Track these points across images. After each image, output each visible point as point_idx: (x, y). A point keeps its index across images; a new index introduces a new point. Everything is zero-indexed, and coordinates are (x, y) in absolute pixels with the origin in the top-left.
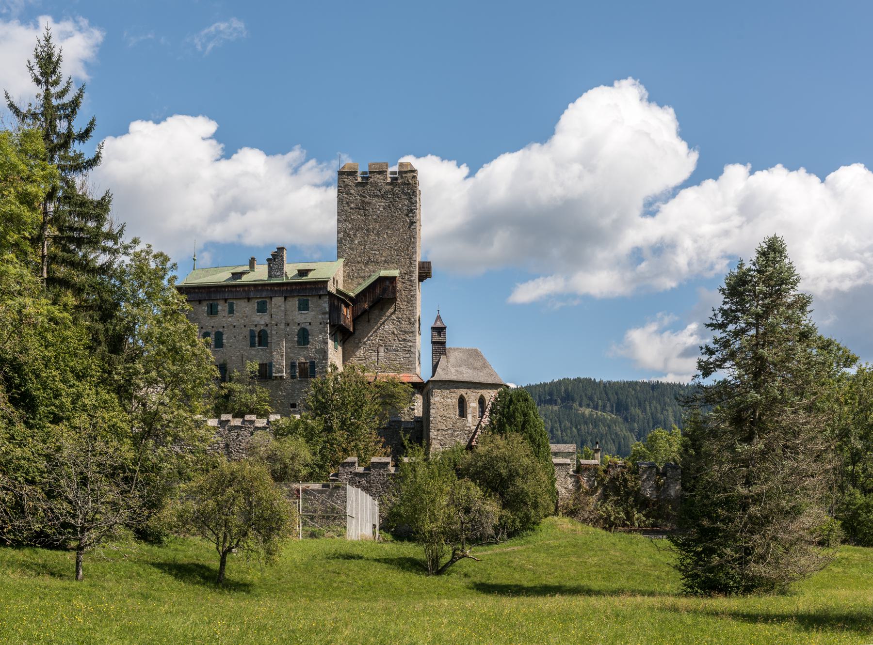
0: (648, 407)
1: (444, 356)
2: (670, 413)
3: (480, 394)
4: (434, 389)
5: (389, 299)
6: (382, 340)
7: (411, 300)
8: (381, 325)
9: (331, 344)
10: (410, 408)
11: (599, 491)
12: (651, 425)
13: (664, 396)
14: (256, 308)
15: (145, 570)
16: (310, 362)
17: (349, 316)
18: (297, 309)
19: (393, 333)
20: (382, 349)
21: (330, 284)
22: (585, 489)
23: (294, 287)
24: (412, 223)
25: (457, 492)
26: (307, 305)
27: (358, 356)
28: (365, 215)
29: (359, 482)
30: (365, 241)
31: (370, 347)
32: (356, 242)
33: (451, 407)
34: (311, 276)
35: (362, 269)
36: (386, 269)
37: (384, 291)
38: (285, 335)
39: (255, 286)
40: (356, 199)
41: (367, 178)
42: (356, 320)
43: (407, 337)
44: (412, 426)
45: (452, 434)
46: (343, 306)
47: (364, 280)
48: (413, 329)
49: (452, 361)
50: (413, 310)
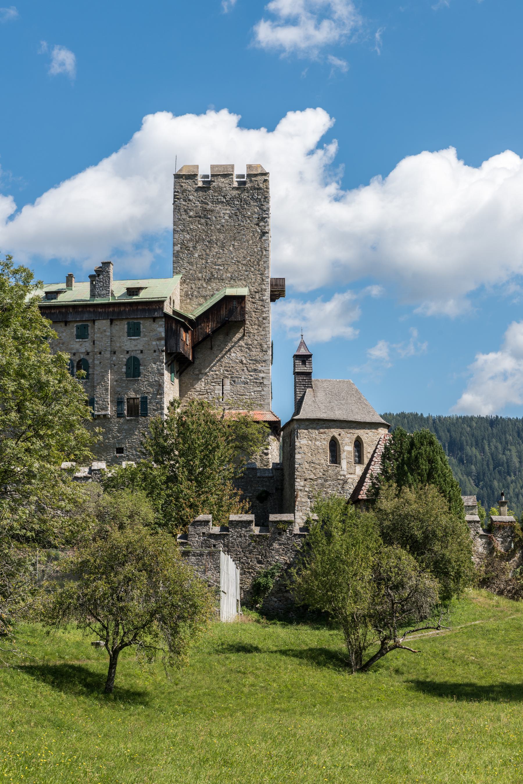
0: (487, 448)
1: (310, 389)
2: (514, 454)
3: (356, 436)
4: (300, 429)
5: (236, 322)
6: (227, 371)
7: (263, 322)
8: (227, 352)
9: (167, 375)
10: (263, 453)
11: (518, 555)
12: (491, 467)
13: (505, 433)
14: (75, 333)
15: (12, 677)
16: (143, 398)
17: (188, 343)
18: (126, 334)
19: (241, 362)
20: (227, 382)
21: (166, 305)
22: (500, 552)
23: (122, 309)
24: (264, 233)
25: (384, 562)
26: (138, 329)
27: (198, 389)
28: (207, 224)
29: (214, 546)
30: (207, 254)
31: (213, 379)
32: (196, 255)
33: (320, 451)
34: (143, 296)
35: (203, 287)
36: (232, 287)
37: (231, 312)
38: (111, 364)
39: (74, 307)
40: (197, 206)
41: (209, 183)
42: (195, 346)
43: (259, 367)
44: (271, 475)
45: (322, 485)
46: (182, 330)
47: (206, 300)
48: (266, 357)
49: (321, 395)
50: (265, 335)
